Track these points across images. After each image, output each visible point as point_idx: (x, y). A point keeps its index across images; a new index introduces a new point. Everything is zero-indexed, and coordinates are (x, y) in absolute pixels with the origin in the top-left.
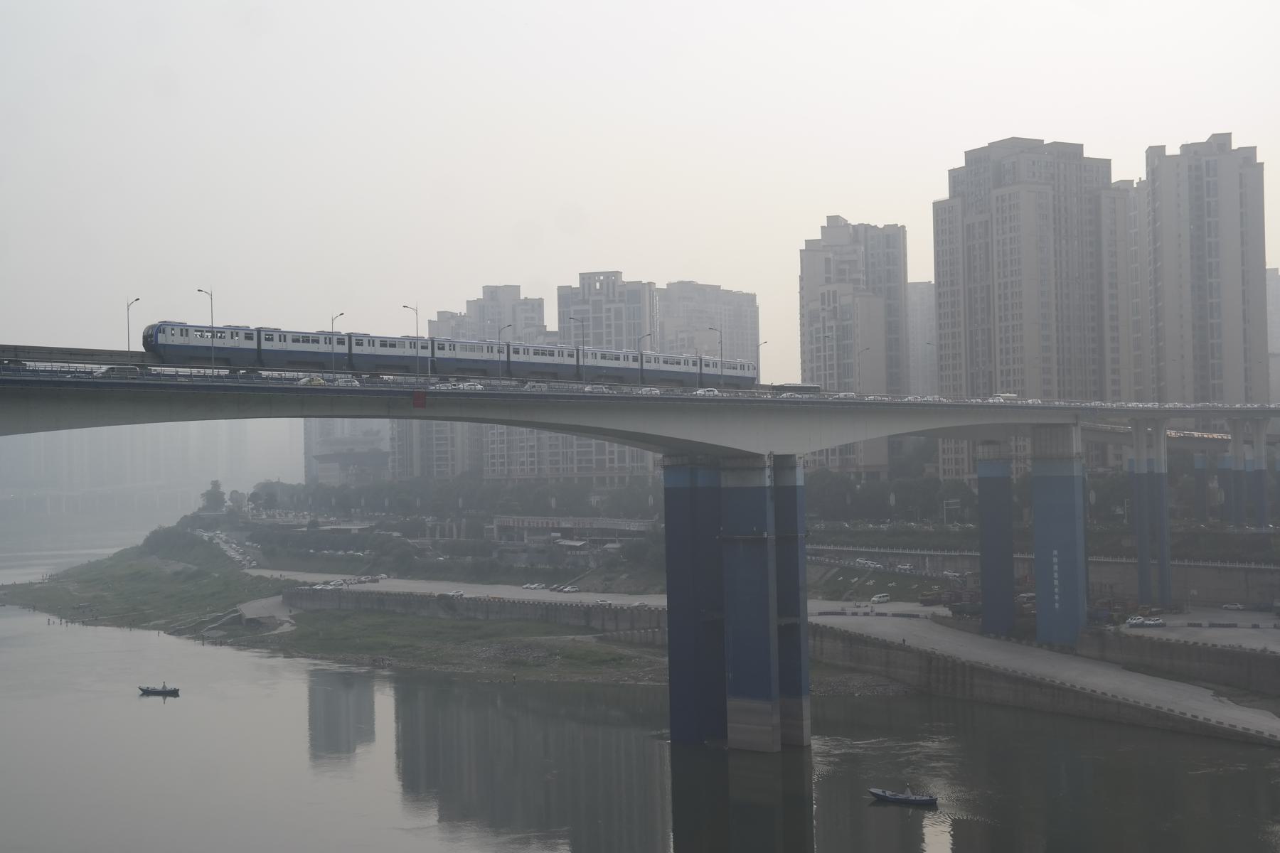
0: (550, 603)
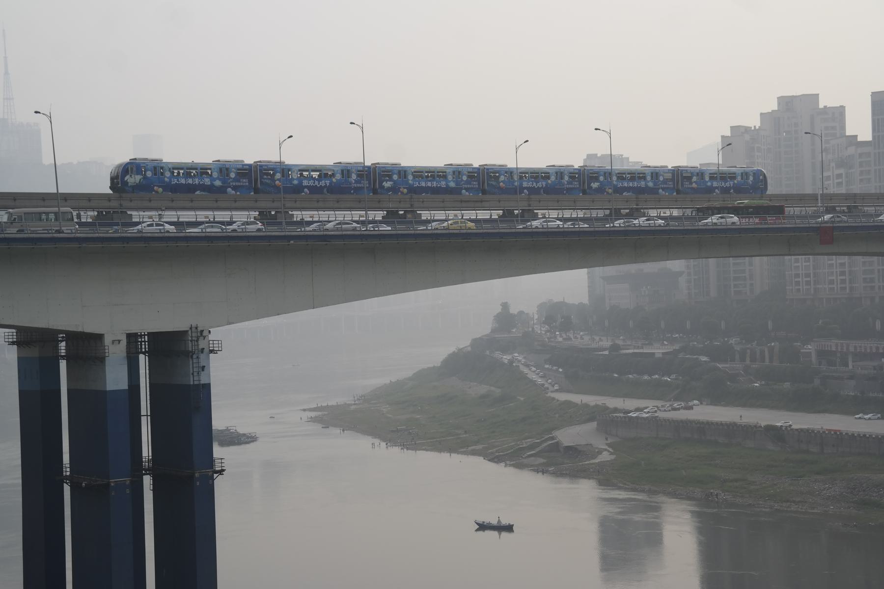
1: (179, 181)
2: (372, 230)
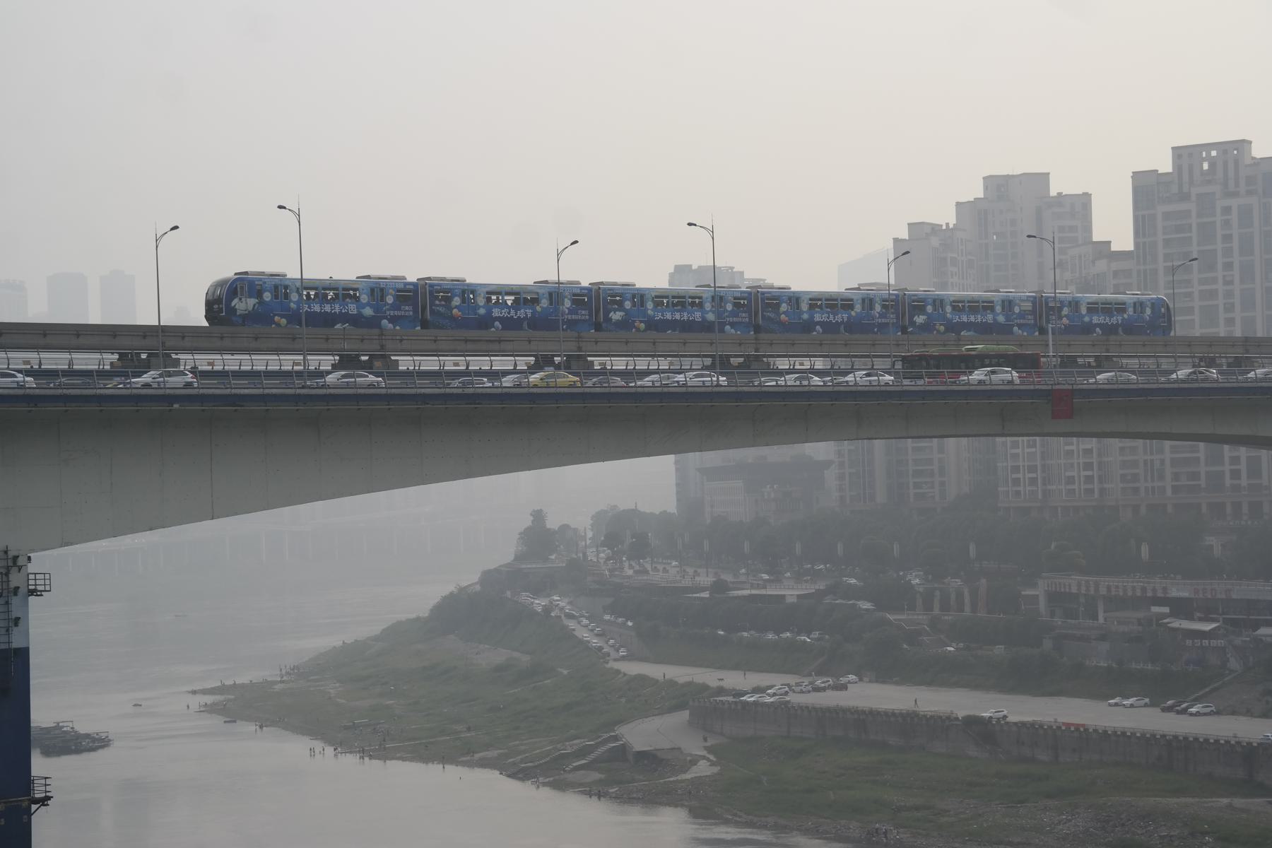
0: (1176, 737)
1: (310, 309)
2: (490, 387)
